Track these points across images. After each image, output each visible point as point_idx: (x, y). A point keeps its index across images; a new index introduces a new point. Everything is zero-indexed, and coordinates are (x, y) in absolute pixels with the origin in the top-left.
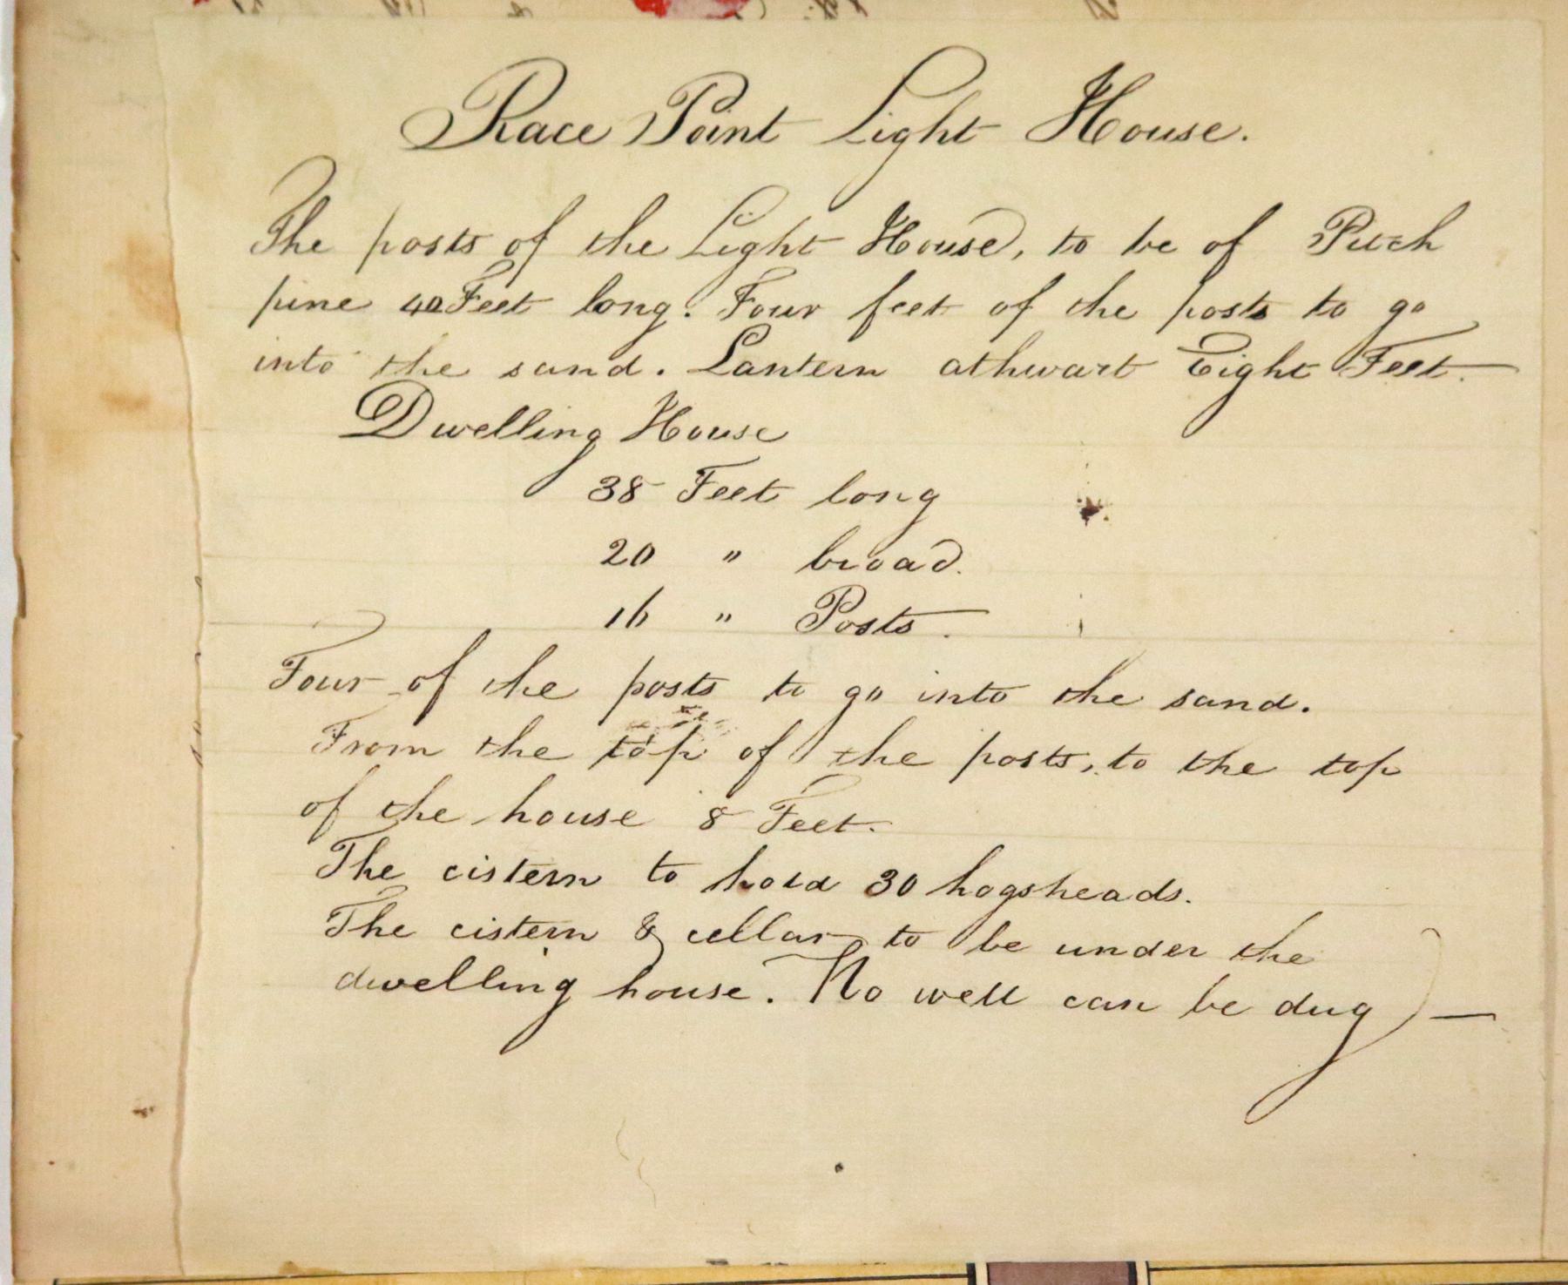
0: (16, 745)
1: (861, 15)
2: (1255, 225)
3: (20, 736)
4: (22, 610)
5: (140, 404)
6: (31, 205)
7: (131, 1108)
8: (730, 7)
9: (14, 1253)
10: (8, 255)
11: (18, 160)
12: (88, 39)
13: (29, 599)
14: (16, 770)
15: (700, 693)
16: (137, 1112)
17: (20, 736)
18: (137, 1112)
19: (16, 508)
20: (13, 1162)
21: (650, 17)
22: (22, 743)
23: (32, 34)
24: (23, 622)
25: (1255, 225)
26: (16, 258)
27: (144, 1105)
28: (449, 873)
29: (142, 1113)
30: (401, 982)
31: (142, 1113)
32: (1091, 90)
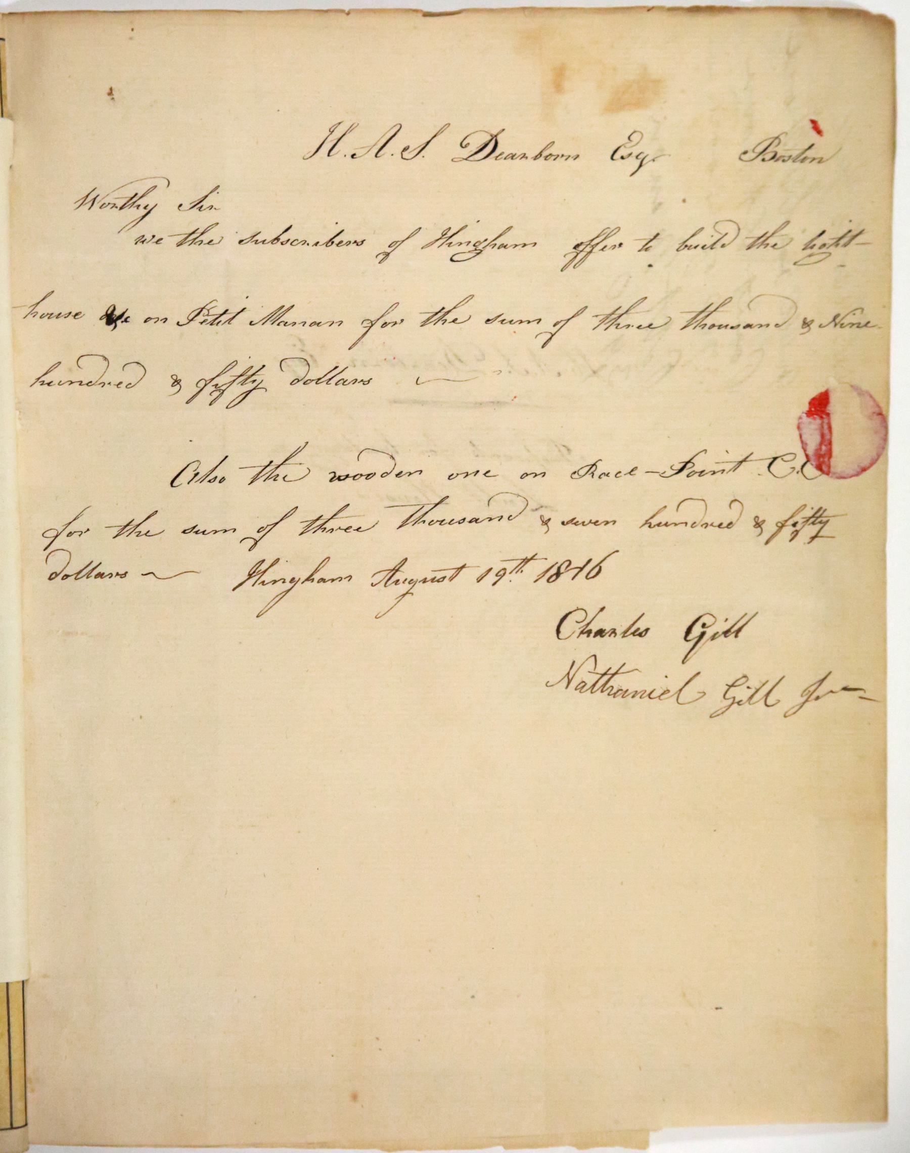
0: (342, 11)
1: (809, 540)
2: (149, 517)
3: (348, 14)
4: (427, 15)
5: (558, 87)
6: (687, 19)
7: (114, 87)
8: (812, 457)
9: (23, 14)
10: (650, 5)
11: (711, 9)
12: (788, 53)
13: (435, 19)
14: (327, 11)
15: (593, 577)
16: (111, 89)
17: (348, 14)
18: (111, 89)
19: (491, 11)
20: (79, 12)
21: (806, 407)
22: (344, 15)
23: (790, 18)
24: (420, 15)
25: (149, 517)
26: (649, 9)
27: (116, 94)
28: (615, 522)
29: (110, 93)
30: (590, 522)
31: (110, 93)
32: (190, 318)
